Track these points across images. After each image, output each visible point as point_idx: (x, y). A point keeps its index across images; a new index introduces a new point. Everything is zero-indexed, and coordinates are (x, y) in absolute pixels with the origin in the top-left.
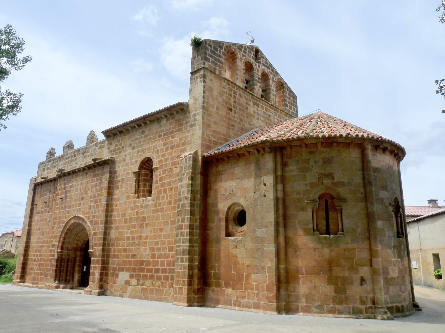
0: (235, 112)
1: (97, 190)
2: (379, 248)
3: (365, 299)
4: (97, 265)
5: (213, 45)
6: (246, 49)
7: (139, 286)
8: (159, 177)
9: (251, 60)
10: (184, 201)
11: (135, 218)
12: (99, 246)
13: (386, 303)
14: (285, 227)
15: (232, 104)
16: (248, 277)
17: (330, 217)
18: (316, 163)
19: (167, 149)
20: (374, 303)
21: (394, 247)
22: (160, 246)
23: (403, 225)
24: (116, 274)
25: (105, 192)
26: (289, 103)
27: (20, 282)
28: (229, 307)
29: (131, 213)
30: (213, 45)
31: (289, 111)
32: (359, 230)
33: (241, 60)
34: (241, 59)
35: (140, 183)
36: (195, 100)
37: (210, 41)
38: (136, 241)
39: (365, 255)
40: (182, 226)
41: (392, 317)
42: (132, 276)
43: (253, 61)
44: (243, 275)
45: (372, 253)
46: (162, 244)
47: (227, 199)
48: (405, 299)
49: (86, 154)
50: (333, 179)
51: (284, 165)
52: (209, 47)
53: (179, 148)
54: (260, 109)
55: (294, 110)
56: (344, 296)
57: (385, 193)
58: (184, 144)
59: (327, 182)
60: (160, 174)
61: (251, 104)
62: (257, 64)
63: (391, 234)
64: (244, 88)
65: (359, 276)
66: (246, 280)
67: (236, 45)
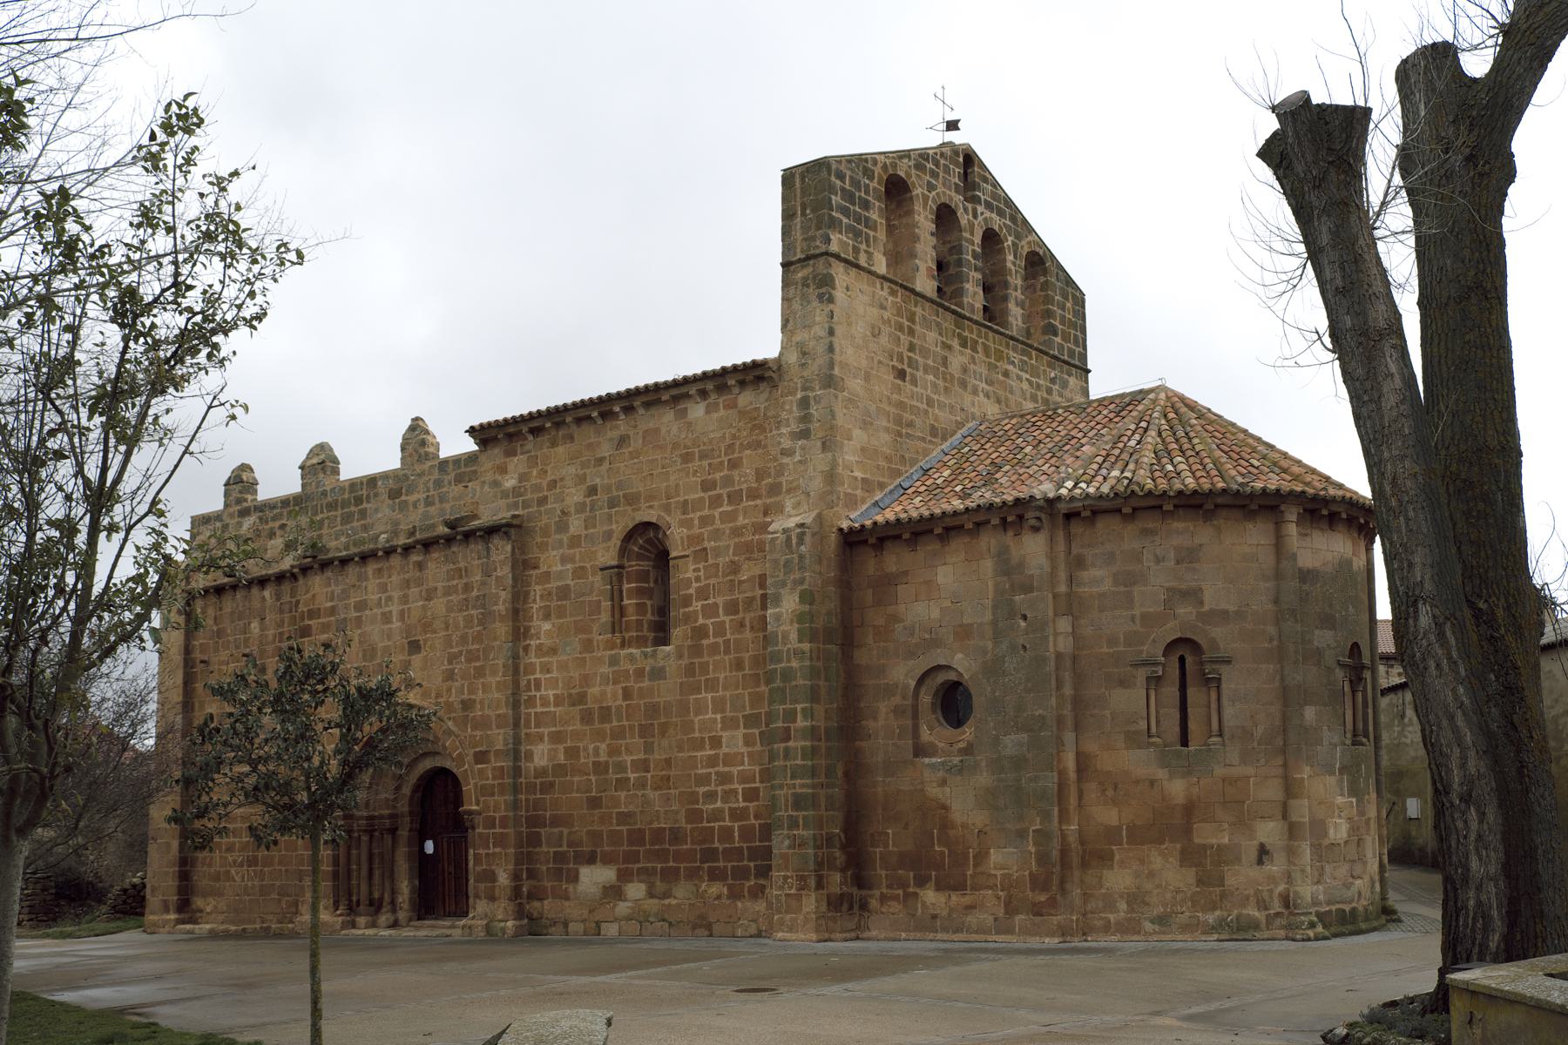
0: (914, 382)
1: (469, 620)
2: (1306, 772)
3: (1266, 895)
4: (498, 850)
5: (848, 173)
6: (937, 164)
7: (656, 901)
8: (695, 585)
9: (951, 199)
10: (789, 661)
11: (619, 708)
12: (502, 793)
13: (1315, 903)
14: (1077, 728)
15: (906, 354)
16: (981, 856)
17: (1189, 700)
18: (1158, 560)
19: (716, 502)
20: (1287, 906)
21: (1343, 770)
22: (713, 787)
23: (1370, 711)
24: (569, 870)
25: (502, 629)
26: (1063, 323)
27: (179, 922)
28: (931, 936)
29: (603, 693)
30: (848, 173)
31: (1061, 347)
32: (1259, 731)
33: (925, 204)
34: (926, 199)
35: (626, 602)
36: (804, 354)
37: (839, 159)
38: (632, 776)
39: (1272, 791)
40: (788, 730)
41: (1327, 933)
42: (624, 876)
43: (957, 199)
44: (965, 855)
45: (1291, 789)
46: (722, 783)
47: (911, 654)
48: (1360, 894)
49: (403, 498)
50: (1202, 603)
51: (1079, 563)
52: (838, 182)
53: (759, 502)
54: (980, 356)
55: (1076, 343)
56: (1218, 889)
57: (1329, 634)
58: (775, 489)
59: (1185, 611)
60: (698, 579)
61: (955, 343)
62: (970, 206)
63: (1336, 739)
64: (934, 296)
65: (1255, 843)
66: (975, 866)
67: (909, 157)
